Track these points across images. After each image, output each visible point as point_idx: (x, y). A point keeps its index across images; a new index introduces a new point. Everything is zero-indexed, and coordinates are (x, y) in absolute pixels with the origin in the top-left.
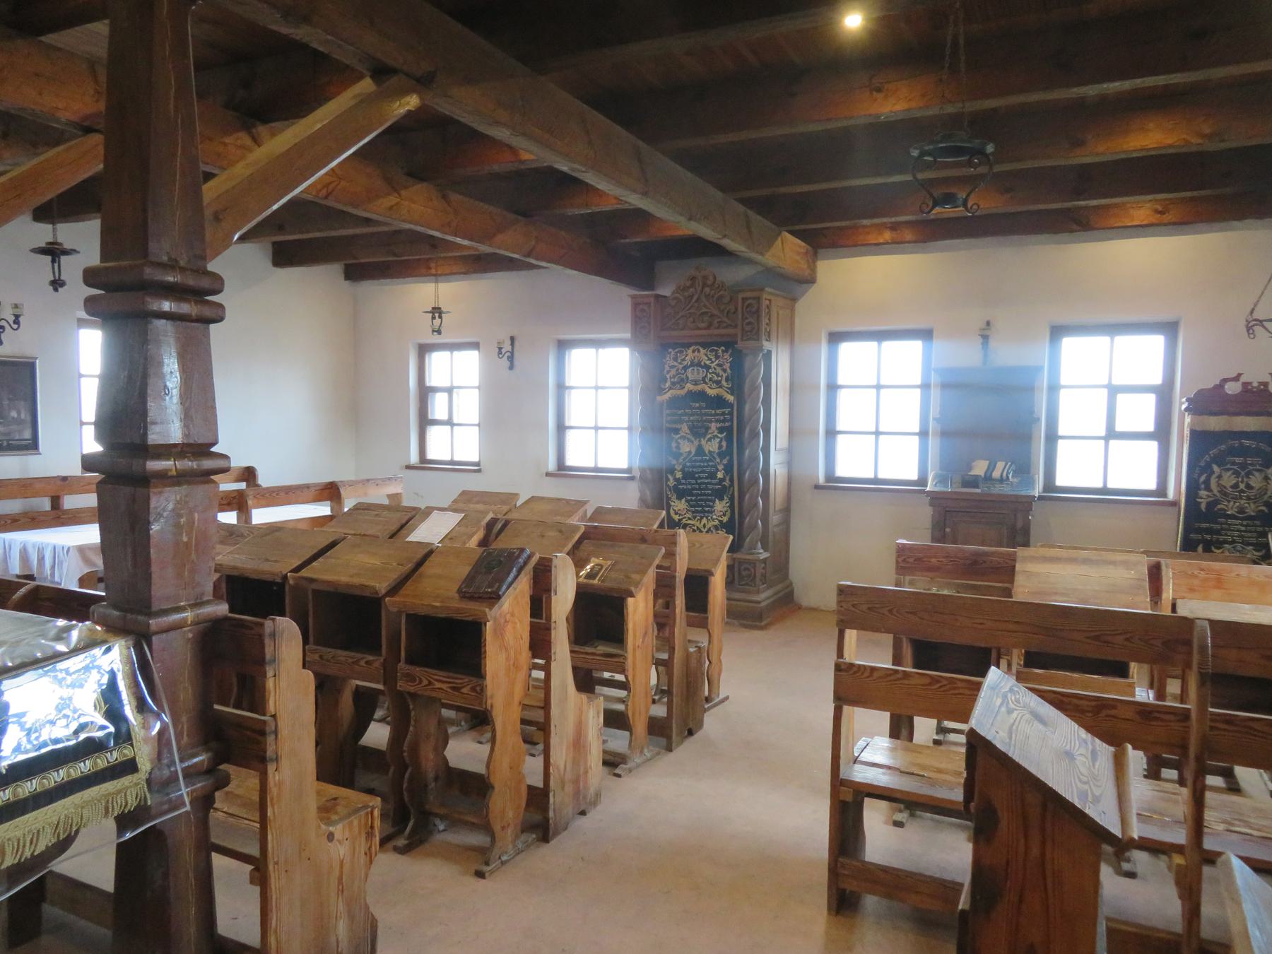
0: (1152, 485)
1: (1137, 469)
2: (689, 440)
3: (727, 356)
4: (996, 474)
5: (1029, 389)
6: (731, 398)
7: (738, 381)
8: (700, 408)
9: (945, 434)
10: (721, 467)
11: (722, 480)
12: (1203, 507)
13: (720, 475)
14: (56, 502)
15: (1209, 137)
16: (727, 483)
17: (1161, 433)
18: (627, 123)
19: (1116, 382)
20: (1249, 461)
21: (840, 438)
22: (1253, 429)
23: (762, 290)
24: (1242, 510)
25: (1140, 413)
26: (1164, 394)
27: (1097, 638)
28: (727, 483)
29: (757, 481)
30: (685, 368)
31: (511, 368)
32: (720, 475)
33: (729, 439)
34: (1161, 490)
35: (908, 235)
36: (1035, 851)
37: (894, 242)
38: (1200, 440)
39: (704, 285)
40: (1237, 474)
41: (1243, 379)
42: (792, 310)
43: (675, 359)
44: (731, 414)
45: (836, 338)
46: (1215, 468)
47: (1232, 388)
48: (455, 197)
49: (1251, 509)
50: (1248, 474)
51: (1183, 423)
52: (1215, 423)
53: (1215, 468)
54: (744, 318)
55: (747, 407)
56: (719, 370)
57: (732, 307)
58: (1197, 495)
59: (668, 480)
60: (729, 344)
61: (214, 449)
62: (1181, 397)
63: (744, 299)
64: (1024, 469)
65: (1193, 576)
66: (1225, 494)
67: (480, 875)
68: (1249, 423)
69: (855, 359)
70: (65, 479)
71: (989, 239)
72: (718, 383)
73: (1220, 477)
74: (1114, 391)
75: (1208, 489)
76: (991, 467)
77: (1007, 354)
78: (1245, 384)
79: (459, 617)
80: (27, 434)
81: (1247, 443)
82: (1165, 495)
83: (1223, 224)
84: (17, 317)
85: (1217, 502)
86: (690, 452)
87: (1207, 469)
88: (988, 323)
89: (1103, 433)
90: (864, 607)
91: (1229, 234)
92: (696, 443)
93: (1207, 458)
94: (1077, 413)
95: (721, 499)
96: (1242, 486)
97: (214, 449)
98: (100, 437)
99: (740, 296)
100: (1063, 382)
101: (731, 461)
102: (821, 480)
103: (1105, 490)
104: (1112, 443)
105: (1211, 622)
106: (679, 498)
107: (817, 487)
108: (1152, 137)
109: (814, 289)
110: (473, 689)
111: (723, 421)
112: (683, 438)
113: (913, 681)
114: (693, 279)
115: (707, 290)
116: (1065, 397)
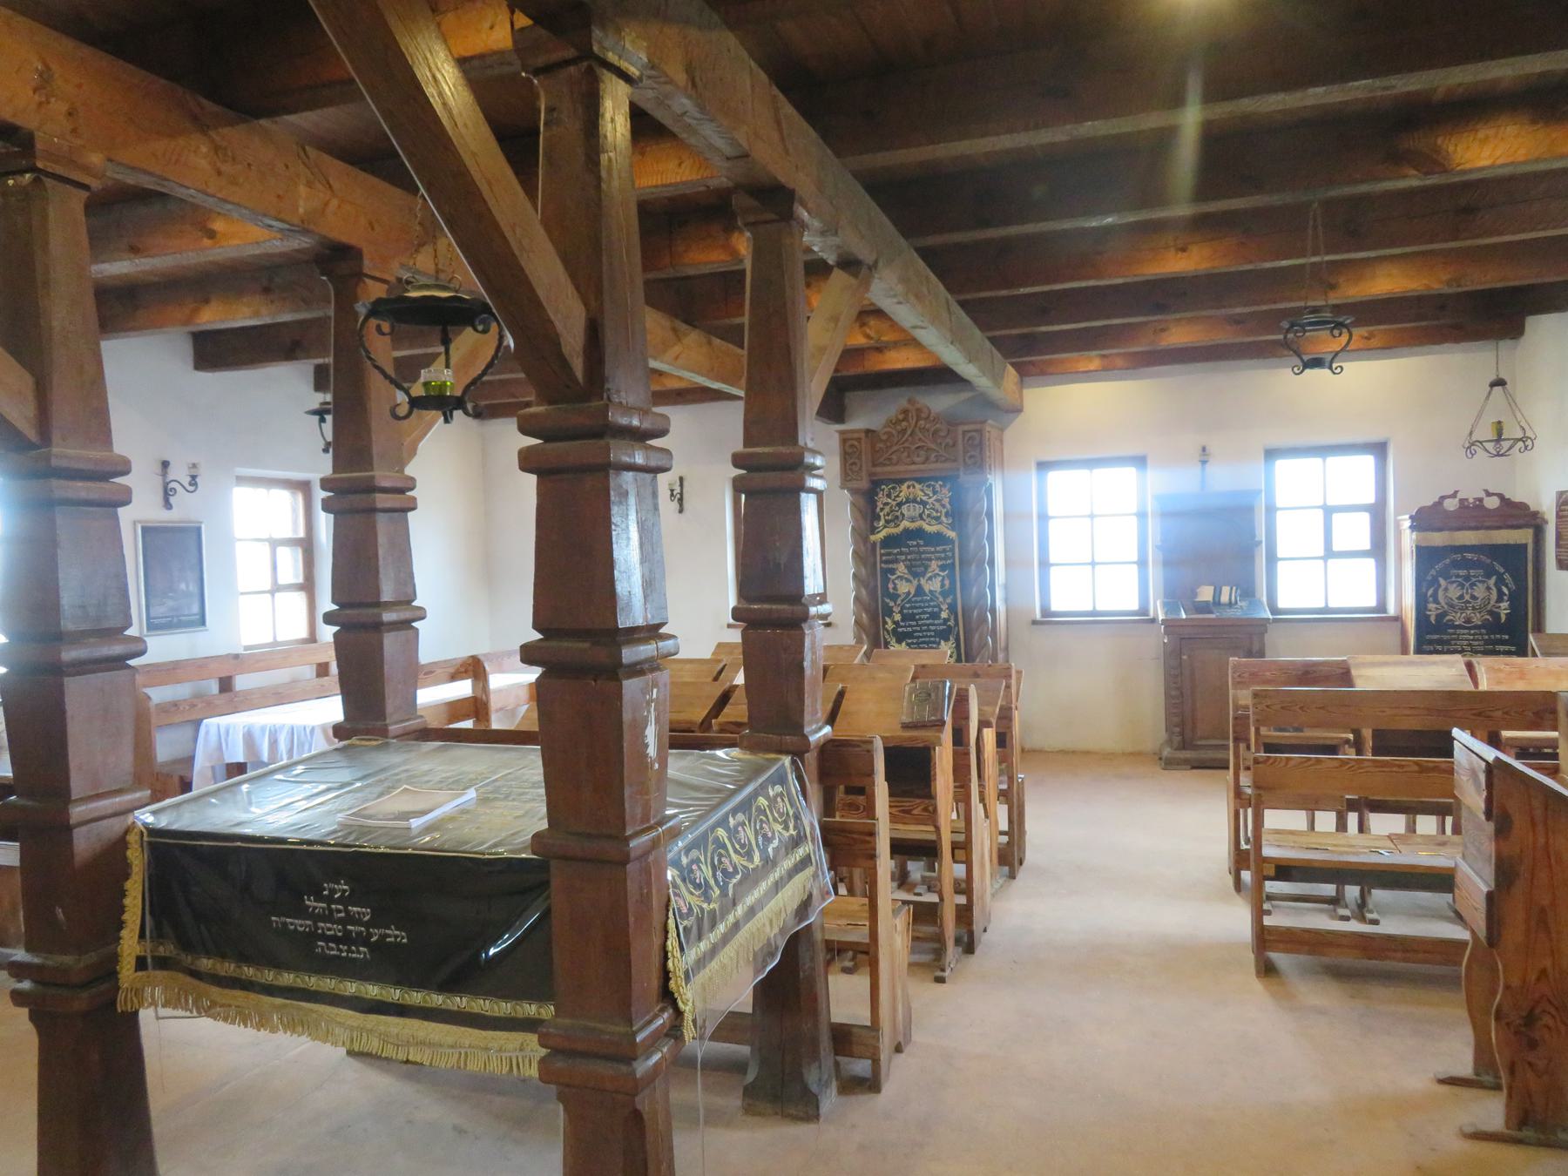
1: (1353, 587)
2: (908, 580)
3: (945, 491)
6: (952, 534)
8: (918, 545)
10: (944, 607)
11: (946, 620)
12: (1433, 619)
13: (944, 615)
14: (226, 685)
16: (951, 623)
17: (1378, 549)
18: (941, 276)
19: (1331, 502)
20: (1472, 572)
21: (1053, 569)
22: (1474, 542)
23: (984, 422)
24: (1468, 620)
25: (1355, 531)
26: (1377, 513)
28: (951, 623)
29: (986, 620)
30: (900, 505)
31: (681, 511)
32: (944, 615)
33: (952, 577)
34: (1381, 607)
35: (1119, 362)
36: (1542, 840)
37: (1105, 369)
38: (1426, 557)
40: (1462, 586)
41: (1460, 496)
43: (889, 496)
44: (952, 550)
45: (1043, 466)
46: (1442, 581)
47: (1451, 505)
49: (1477, 619)
50: (1473, 584)
52: (1438, 539)
53: (1442, 581)
54: (965, 452)
56: (937, 505)
58: (1426, 608)
59: (885, 623)
63: (964, 432)
64: (1248, 592)
65: (1500, 670)
66: (1452, 606)
69: (1066, 490)
70: (236, 656)
71: (1199, 365)
72: (937, 519)
73: (1446, 589)
75: (1436, 601)
78: (1461, 501)
80: (195, 609)
81: (1469, 556)
82: (1385, 611)
84: (194, 477)
85: (1445, 614)
87: (1434, 582)
88: (1204, 449)
89: (1322, 553)
90: (1278, 707)
91: (1430, 358)
92: (915, 582)
93: (1433, 572)
94: (1294, 535)
95: (947, 640)
96: (1467, 597)
98: (334, 601)
99: (961, 429)
100: (1278, 505)
101: (955, 600)
102: (1038, 616)
103: (1326, 610)
104: (1330, 561)
106: (899, 641)
107: (1035, 622)
109: (1021, 417)
112: (901, 578)
114: (905, 412)
116: (1281, 519)
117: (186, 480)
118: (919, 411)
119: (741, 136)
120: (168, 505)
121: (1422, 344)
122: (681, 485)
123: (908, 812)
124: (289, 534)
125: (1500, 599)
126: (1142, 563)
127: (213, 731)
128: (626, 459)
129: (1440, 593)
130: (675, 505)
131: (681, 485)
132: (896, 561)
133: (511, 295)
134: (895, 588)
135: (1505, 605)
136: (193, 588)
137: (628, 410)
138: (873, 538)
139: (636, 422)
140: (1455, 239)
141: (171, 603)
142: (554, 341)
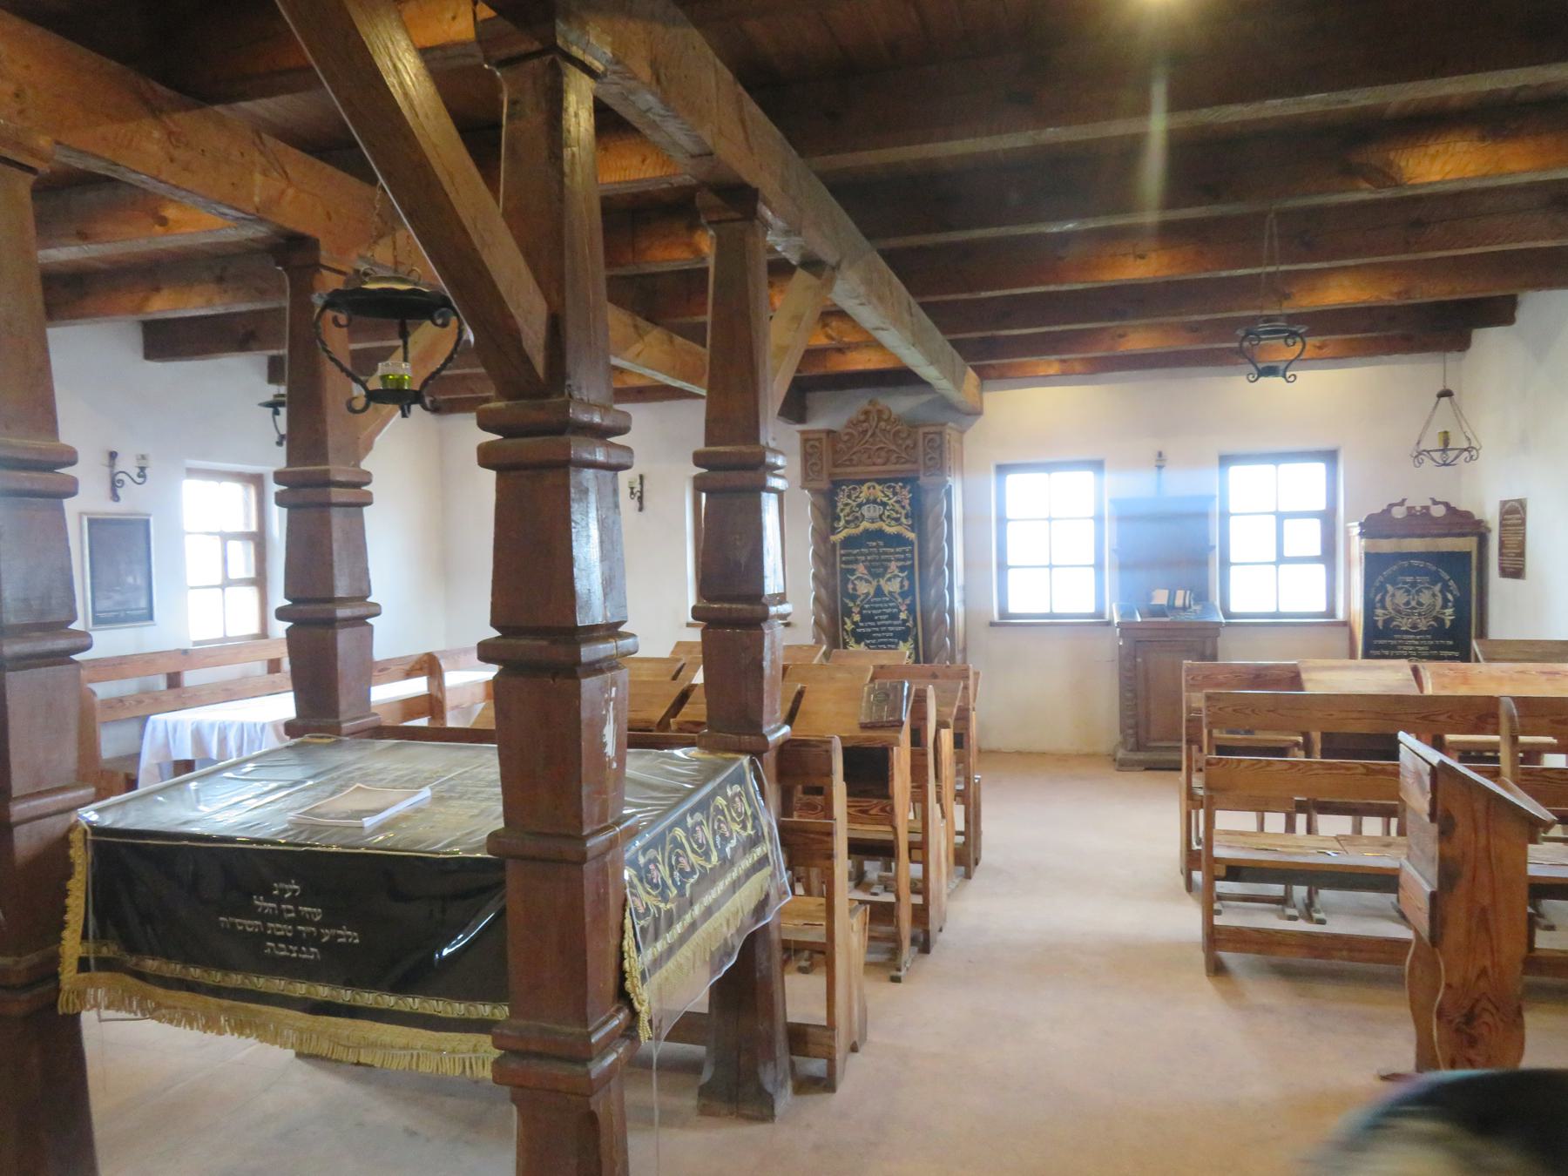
0: (1321, 607)
1: (1304, 592)
2: (867, 581)
3: (905, 492)
4: (1179, 602)
5: (1203, 516)
6: (911, 536)
7: (917, 516)
8: (878, 546)
9: (1124, 567)
10: (903, 608)
11: (905, 621)
13: (903, 616)
14: (174, 681)
15: (1399, 294)
17: (1328, 555)
19: (1282, 509)
20: (1419, 579)
23: (944, 425)
24: (1414, 626)
26: (1328, 519)
27: (1424, 718)
28: (910, 624)
30: (860, 506)
31: (641, 509)
32: (903, 616)
33: (911, 578)
34: (1331, 612)
37: (1064, 373)
38: (1374, 562)
39: (880, 419)
40: (1408, 591)
41: (1407, 504)
42: (961, 443)
43: (849, 497)
44: (912, 552)
45: (1002, 469)
46: (1389, 587)
47: (1399, 513)
48: (679, 340)
49: (1423, 626)
50: (1418, 592)
51: (1356, 546)
52: (1386, 546)
53: (1389, 587)
54: (926, 454)
55: (931, 546)
56: (897, 507)
57: (909, 442)
58: (1373, 614)
59: (844, 623)
60: (909, 480)
61: (72, 627)
62: (1348, 520)
63: (925, 434)
64: (1201, 596)
65: (1445, 675)
66: (1399, 612)
67: (896, 980)
68: (1416, 545)
70: (185, 652)
72: (897, 520)
74: (1281, 517)
75: (1384, 607)
76: (1172, 597)
77: (1183, 483)
79: (867, 745)
80: (143, 603)
83: (1375, 359)
84: (142, 469)
85: (1392, 619)
86: (867, 594)
87: (1382, 589)
88: (1160, 454)
92: (875, 583)
94: (1247, 540)
95: (905, 641)
97: (72, 627)
98: (287, 597)
99: (921, 431)
101: (913, 601)
102: (996, 618)
104: (1282, 567)
105: (1513, 698)
106: (858, 642)
107: (992, 624)
108: (1339, 293)
109: (979, 423)
110: (883, 810)
111: (905, 560)
112: (860, 578)
113: (1275, 768)
114: (867, 413)
115: (883, 424)
117: (134, 472)
118: (880, 412)
119: (707, 135)
120: (115, 497)
121: (1366, 355)
122: (641, 484)
123: (864, 812)
124: (241, 528)
125: (1445, 606)
126: (1099, 566)
127: (160, 728)
128: (587, 456)
129: (1388, 599)
130: (635, 503)
131: (641, 484)
132: (856, 562)
133: (471, 288)
134: (855, 589)
135: (1449, 611)
136: (140, 581)
137: (589, 407)
138: (833, 538)
139: (597, 419)
140: (1405, 252)
141: (117, 597)
142: (515, 335)
